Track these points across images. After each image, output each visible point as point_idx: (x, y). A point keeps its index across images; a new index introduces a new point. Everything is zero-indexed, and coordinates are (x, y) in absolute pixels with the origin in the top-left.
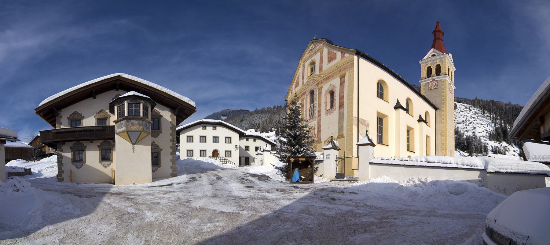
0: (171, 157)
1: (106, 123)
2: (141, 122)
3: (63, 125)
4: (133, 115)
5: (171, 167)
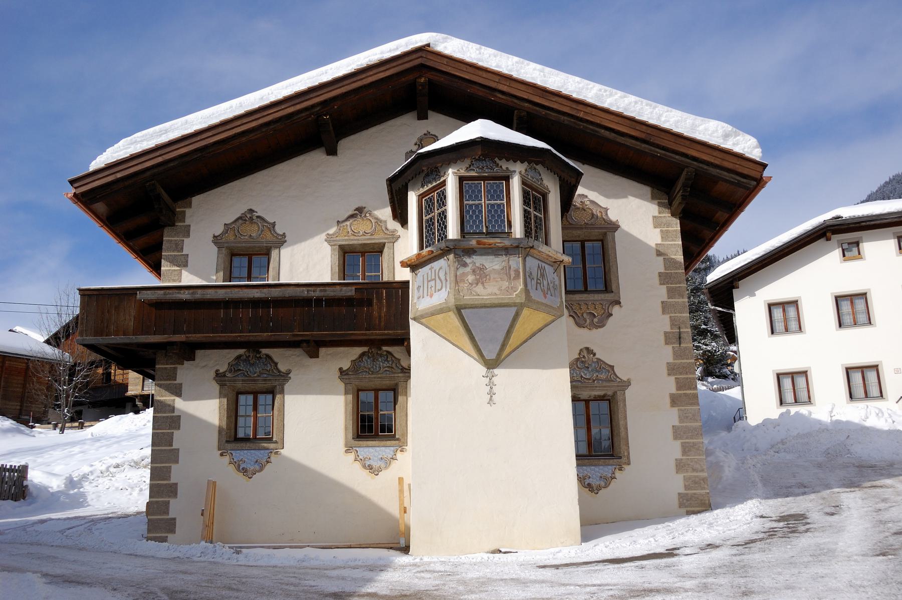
0: (672, 416)
1: (377, 267)
2: (516, 262)
3: (195, 270)
4: (481, 237)
5: (680, 466)
